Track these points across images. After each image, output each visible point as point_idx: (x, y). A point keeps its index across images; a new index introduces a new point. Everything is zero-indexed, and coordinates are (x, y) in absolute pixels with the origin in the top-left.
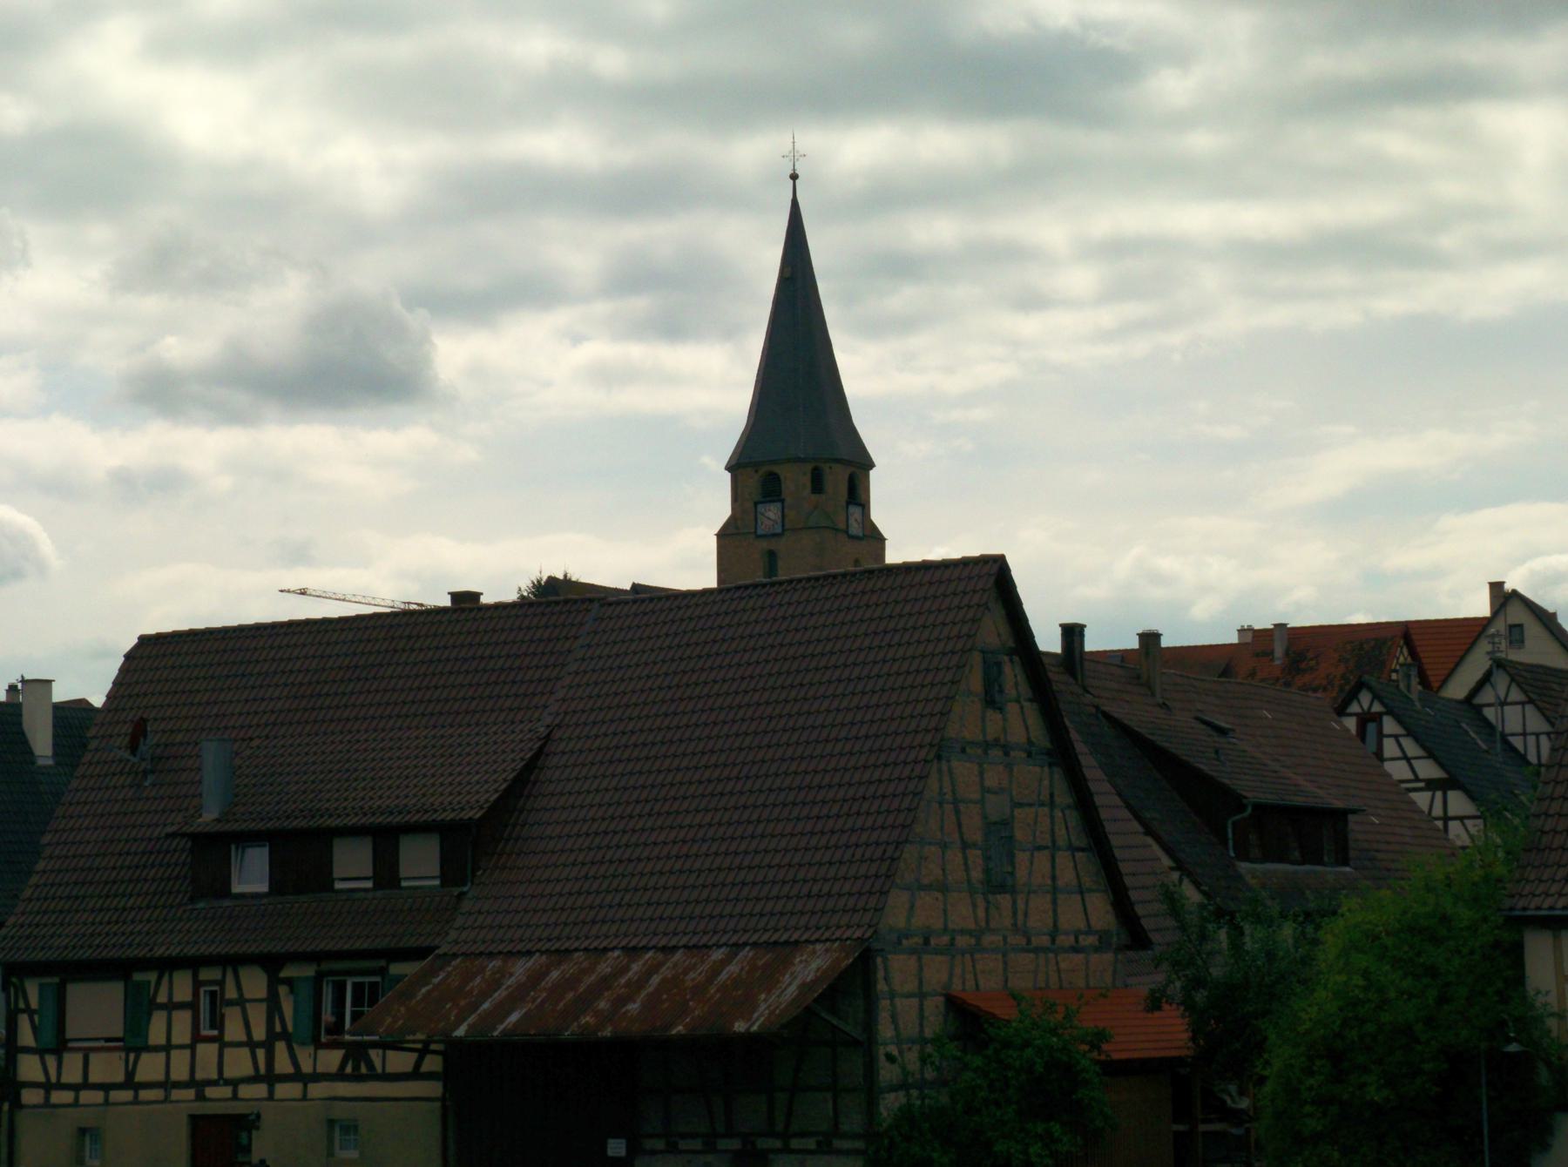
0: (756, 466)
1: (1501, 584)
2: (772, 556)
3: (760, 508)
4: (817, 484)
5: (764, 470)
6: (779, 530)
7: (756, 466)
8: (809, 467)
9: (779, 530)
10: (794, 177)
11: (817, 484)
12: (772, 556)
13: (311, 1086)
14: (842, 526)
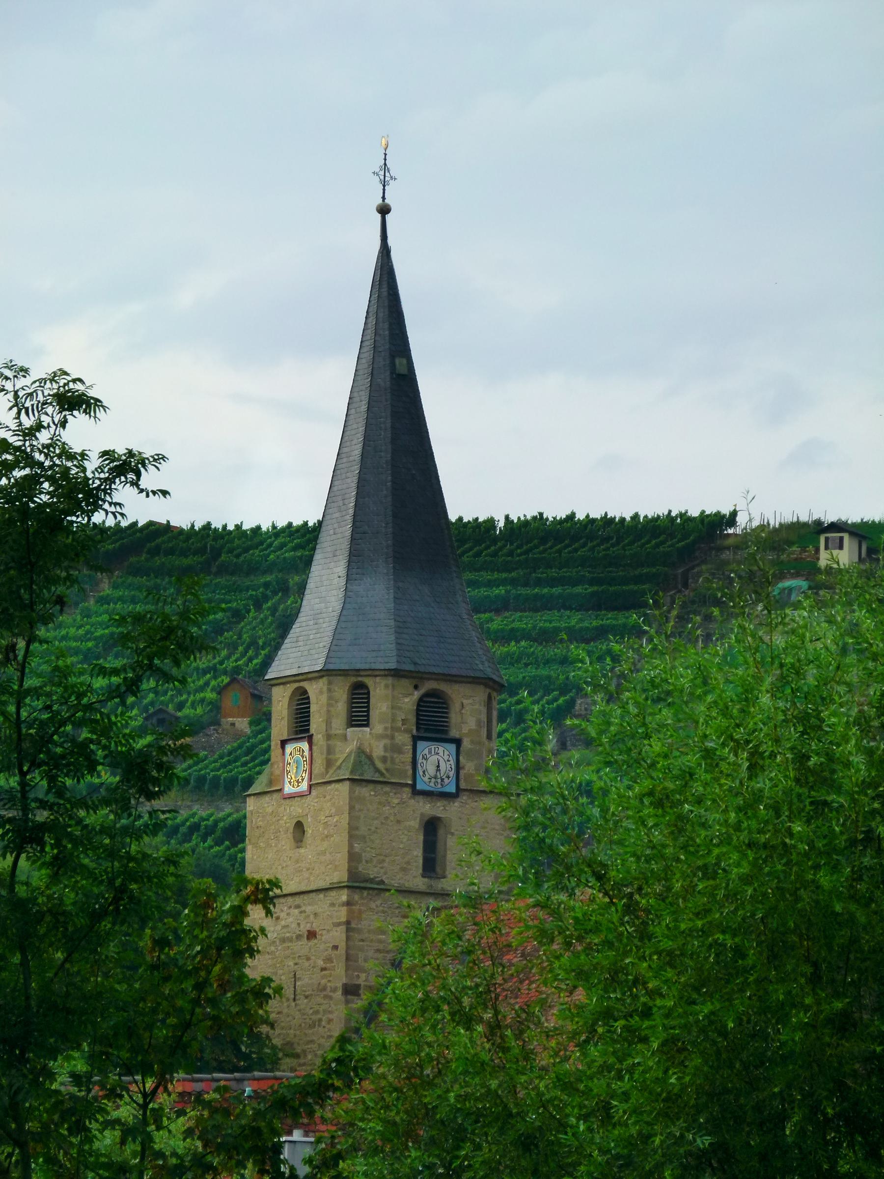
6: (452, 789)
7: (344, 673)
10: (384, 210)
12: (432, 828)
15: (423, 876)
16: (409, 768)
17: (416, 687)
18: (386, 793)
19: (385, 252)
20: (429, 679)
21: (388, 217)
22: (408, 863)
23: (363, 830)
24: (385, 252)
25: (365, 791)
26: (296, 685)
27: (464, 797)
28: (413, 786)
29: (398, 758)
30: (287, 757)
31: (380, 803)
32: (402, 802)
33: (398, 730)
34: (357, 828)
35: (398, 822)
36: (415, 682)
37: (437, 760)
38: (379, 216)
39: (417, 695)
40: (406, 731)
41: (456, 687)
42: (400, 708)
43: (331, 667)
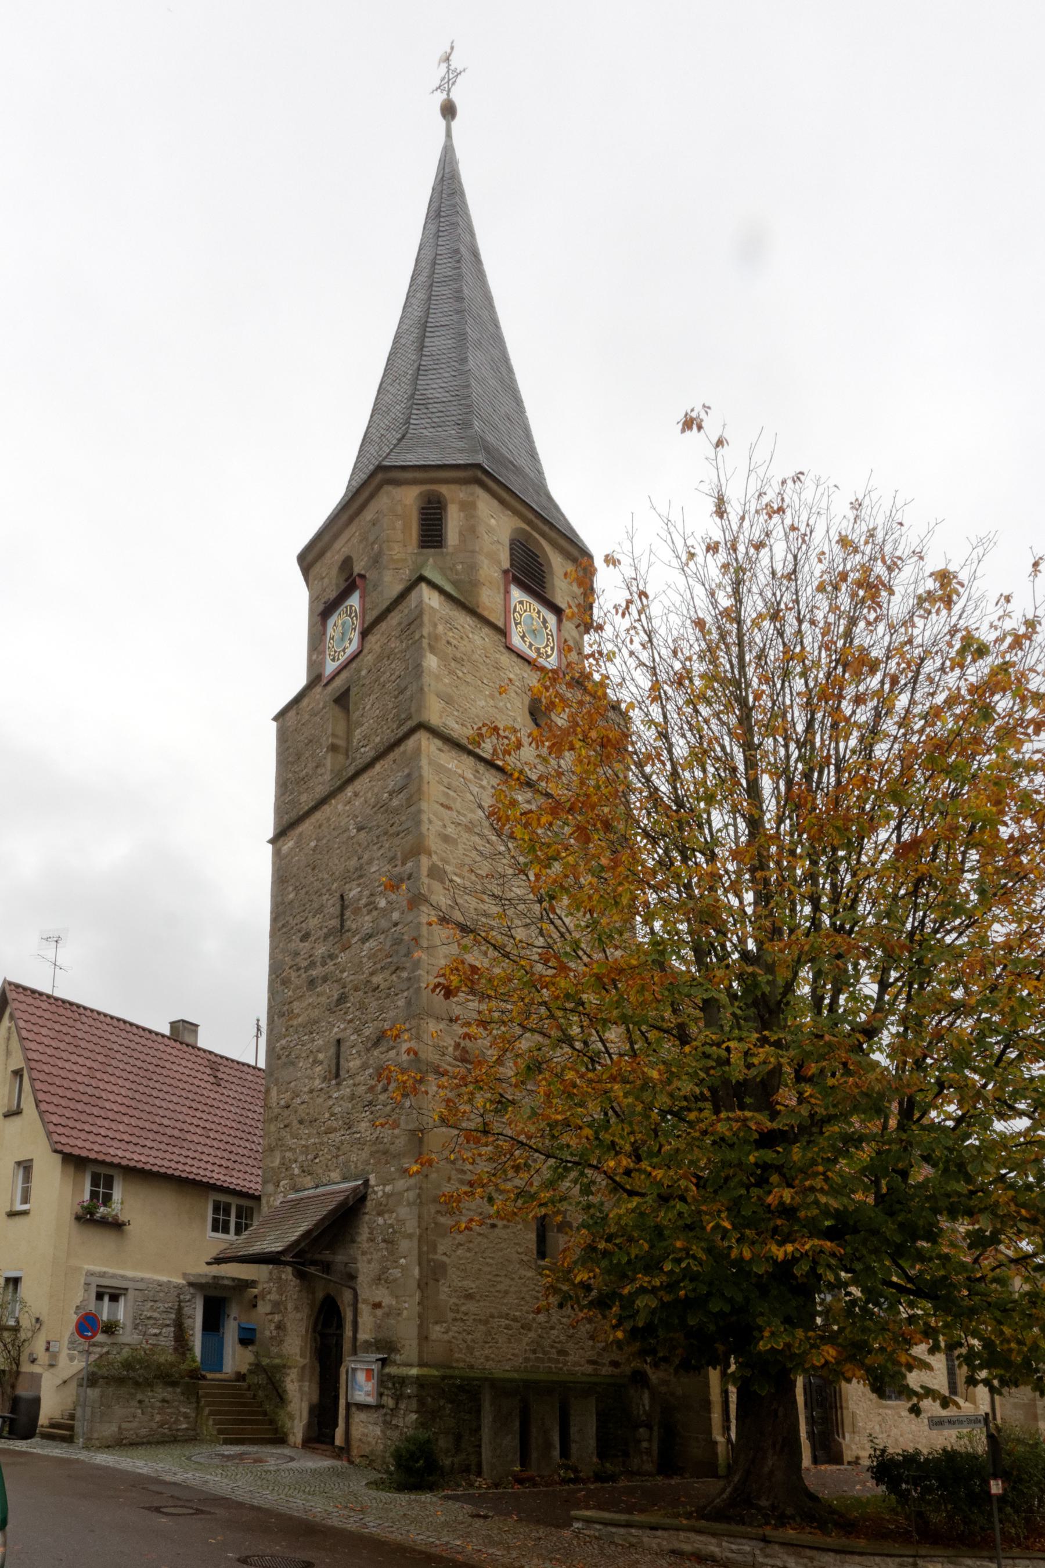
21: (454, 124)
30: (330, 631)
38: (443, 123)
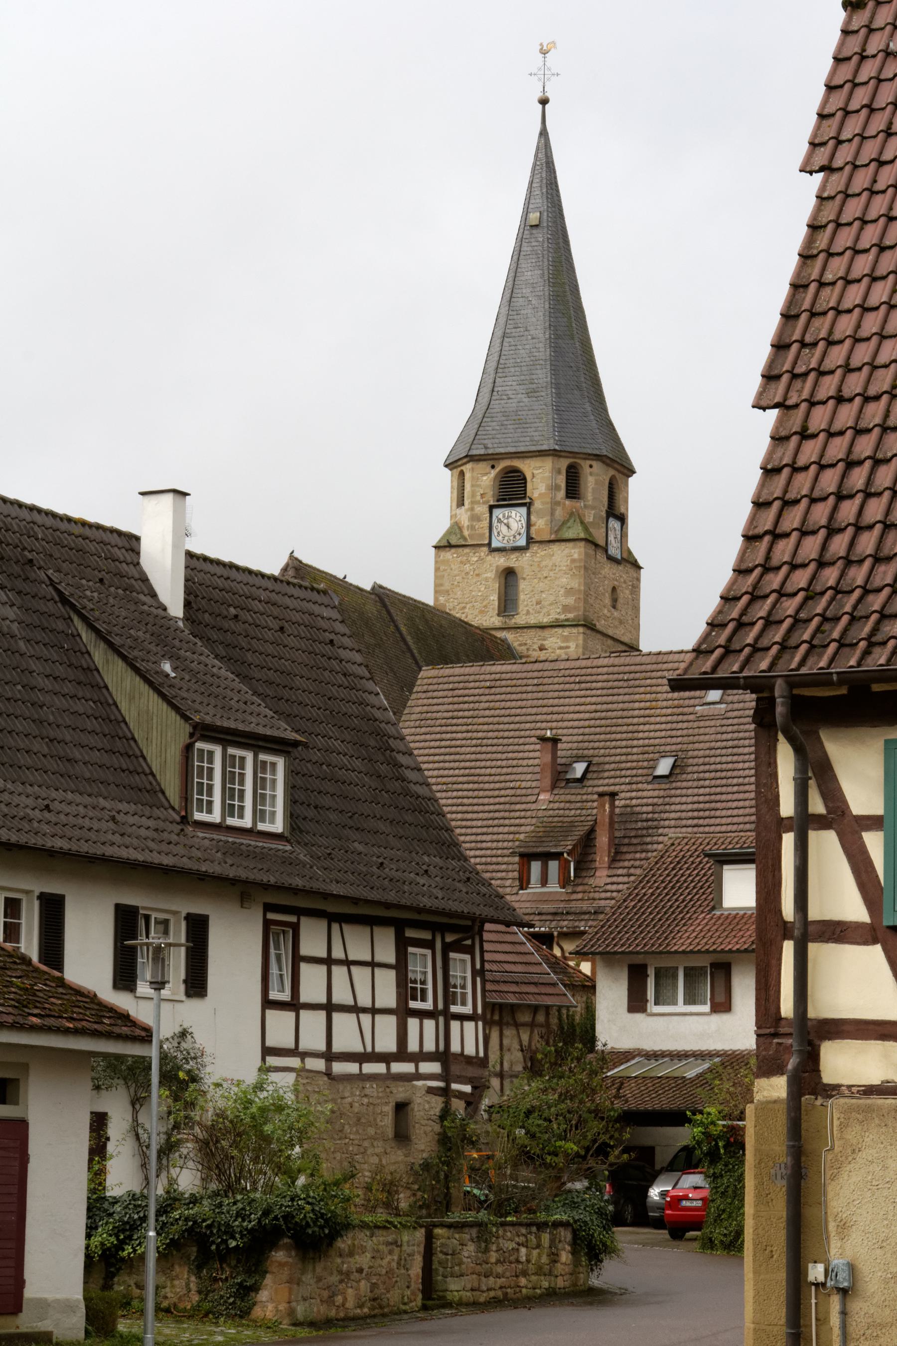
0: (491, 458)
1: (555, 47)
2: (509, 575)
3: (497, 512)
4: (573, 490)
5: (502, 465)
6: (522, 542)
7: (491, 458)
8: (564, 463)
9: (522, 542)
10: (544, 102)
11: (573, 490)
12: (509, 575)
13: (392, 974)
14: (602, 543)
15: (499, 615)
16: (487, 531)
17: (493, 467)
18: (468, 554)
19: (544, 133)
20: (503, 459)
22: (485, 606)
23: (447, 586)
24: (544, 133)
25: (448, 555)
26: (572, 460)
27: (534, 548)
28: (489, 544)
29: (477, 525)
31: (461, 562)
32: (480, 559)
33: (478, 503)
34: (442, 585)
35: (478, 575)
36: (491, 463)
37: (514, 520)
38: (541, 106)
39: (493, 473)
40: (484, 503)
41: (528, 461)
42: (479, 486)
43: (474, 452)
